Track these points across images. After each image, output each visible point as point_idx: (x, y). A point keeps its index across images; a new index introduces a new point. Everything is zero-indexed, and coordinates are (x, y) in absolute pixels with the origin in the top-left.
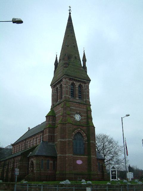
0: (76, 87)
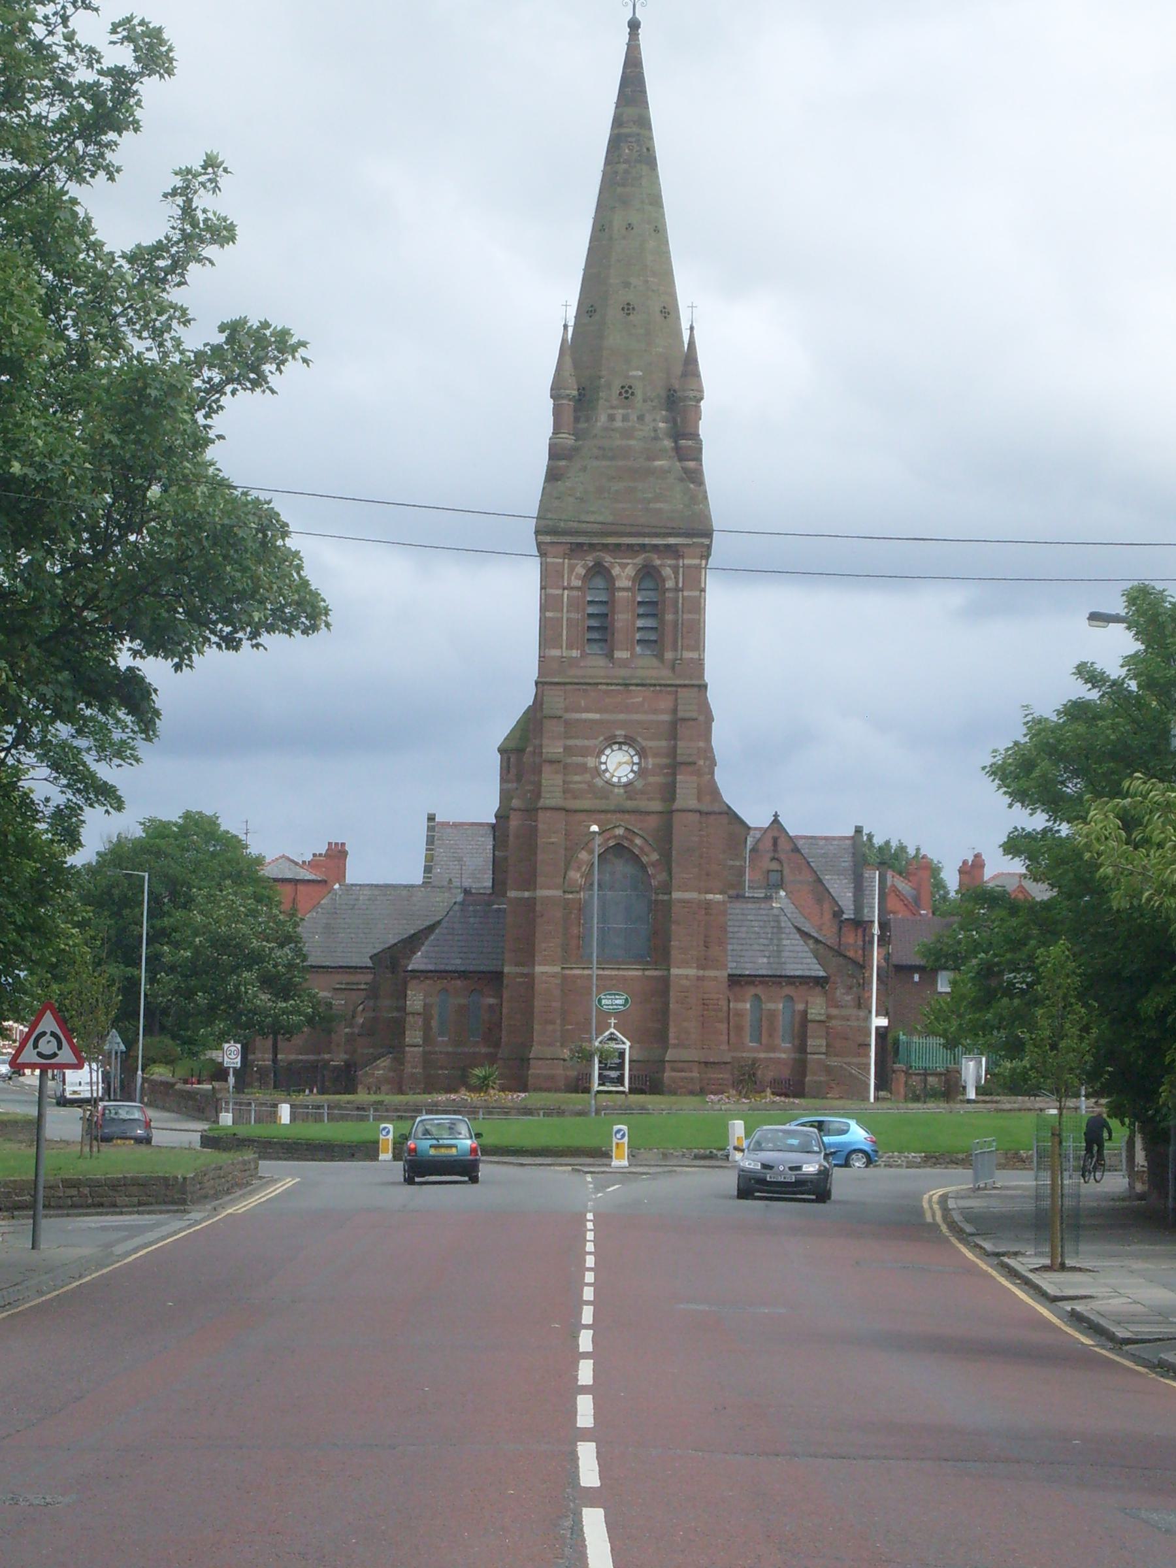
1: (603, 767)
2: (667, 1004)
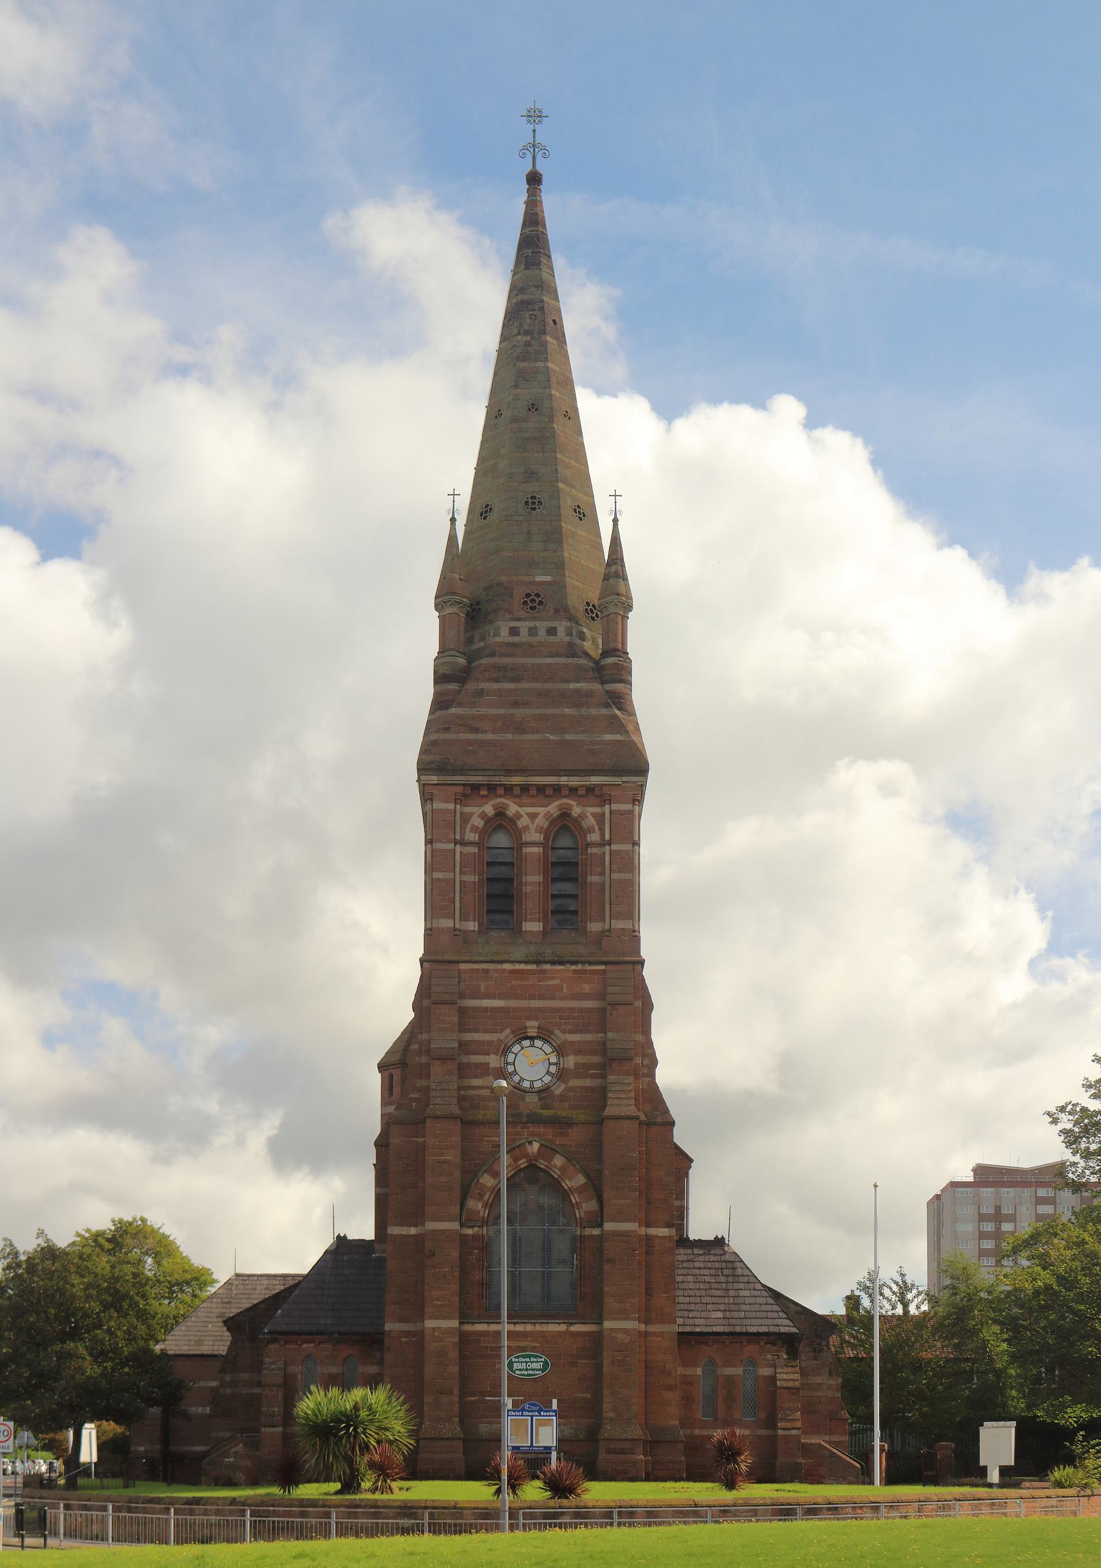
1: (510, 1069)
2: (599, 1367)
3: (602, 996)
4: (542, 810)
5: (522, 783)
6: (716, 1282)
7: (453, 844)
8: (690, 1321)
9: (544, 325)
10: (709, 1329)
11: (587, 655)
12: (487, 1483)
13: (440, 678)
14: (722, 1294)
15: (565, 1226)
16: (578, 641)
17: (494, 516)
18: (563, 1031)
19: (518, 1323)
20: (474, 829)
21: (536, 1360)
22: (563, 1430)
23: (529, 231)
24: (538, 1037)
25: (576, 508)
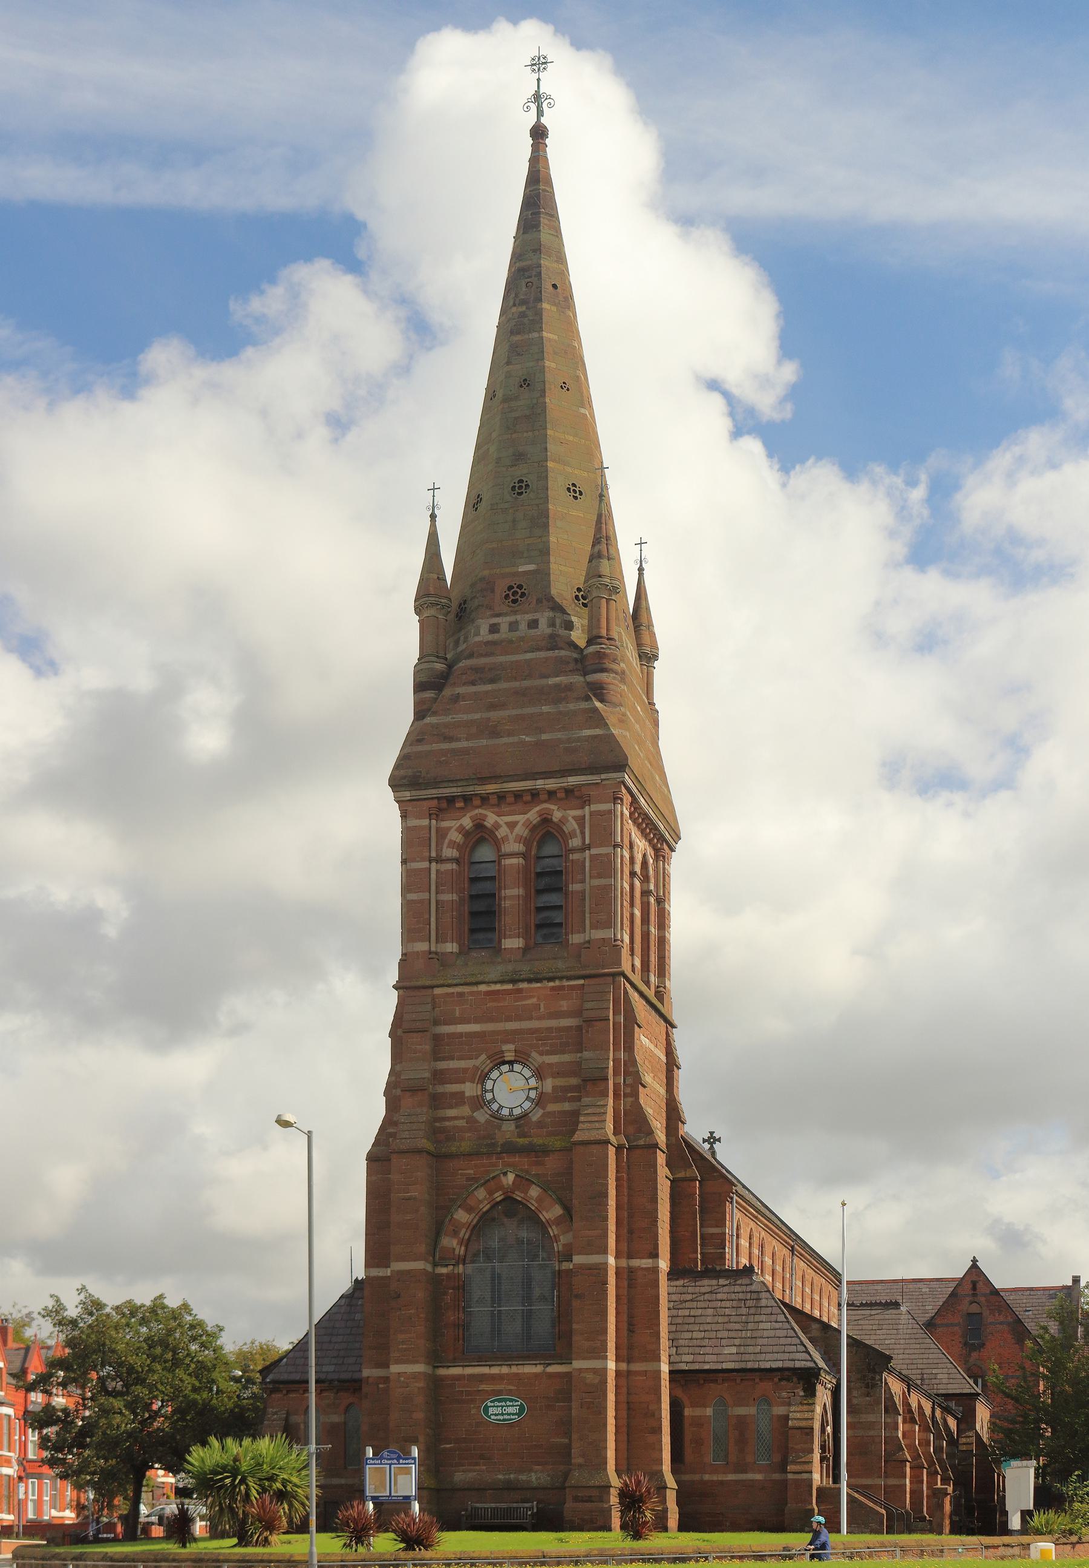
0: (507, 848)
1: (489, 1096)
3: (578, 1013)
4: (521, 818)
5: (496, 791)
6: (737, 1315)
7: (428, 863)
8: (700, 1358)
9: (541, 292)
10: (719, 1367)
11: (573, 646)
12: (333, 1535)
13: (419, 687)
14: (740, 1328)
15: (546, 1261)
16: (562, 632)
17: (482, 506)
18: (541, 1054)
19: (493, 1365)
20: (453, 844)
21: (511, 1404)
22: (540, 1478)
23: (530, 191)
24: (516, 1061)
25: (571, 487)
